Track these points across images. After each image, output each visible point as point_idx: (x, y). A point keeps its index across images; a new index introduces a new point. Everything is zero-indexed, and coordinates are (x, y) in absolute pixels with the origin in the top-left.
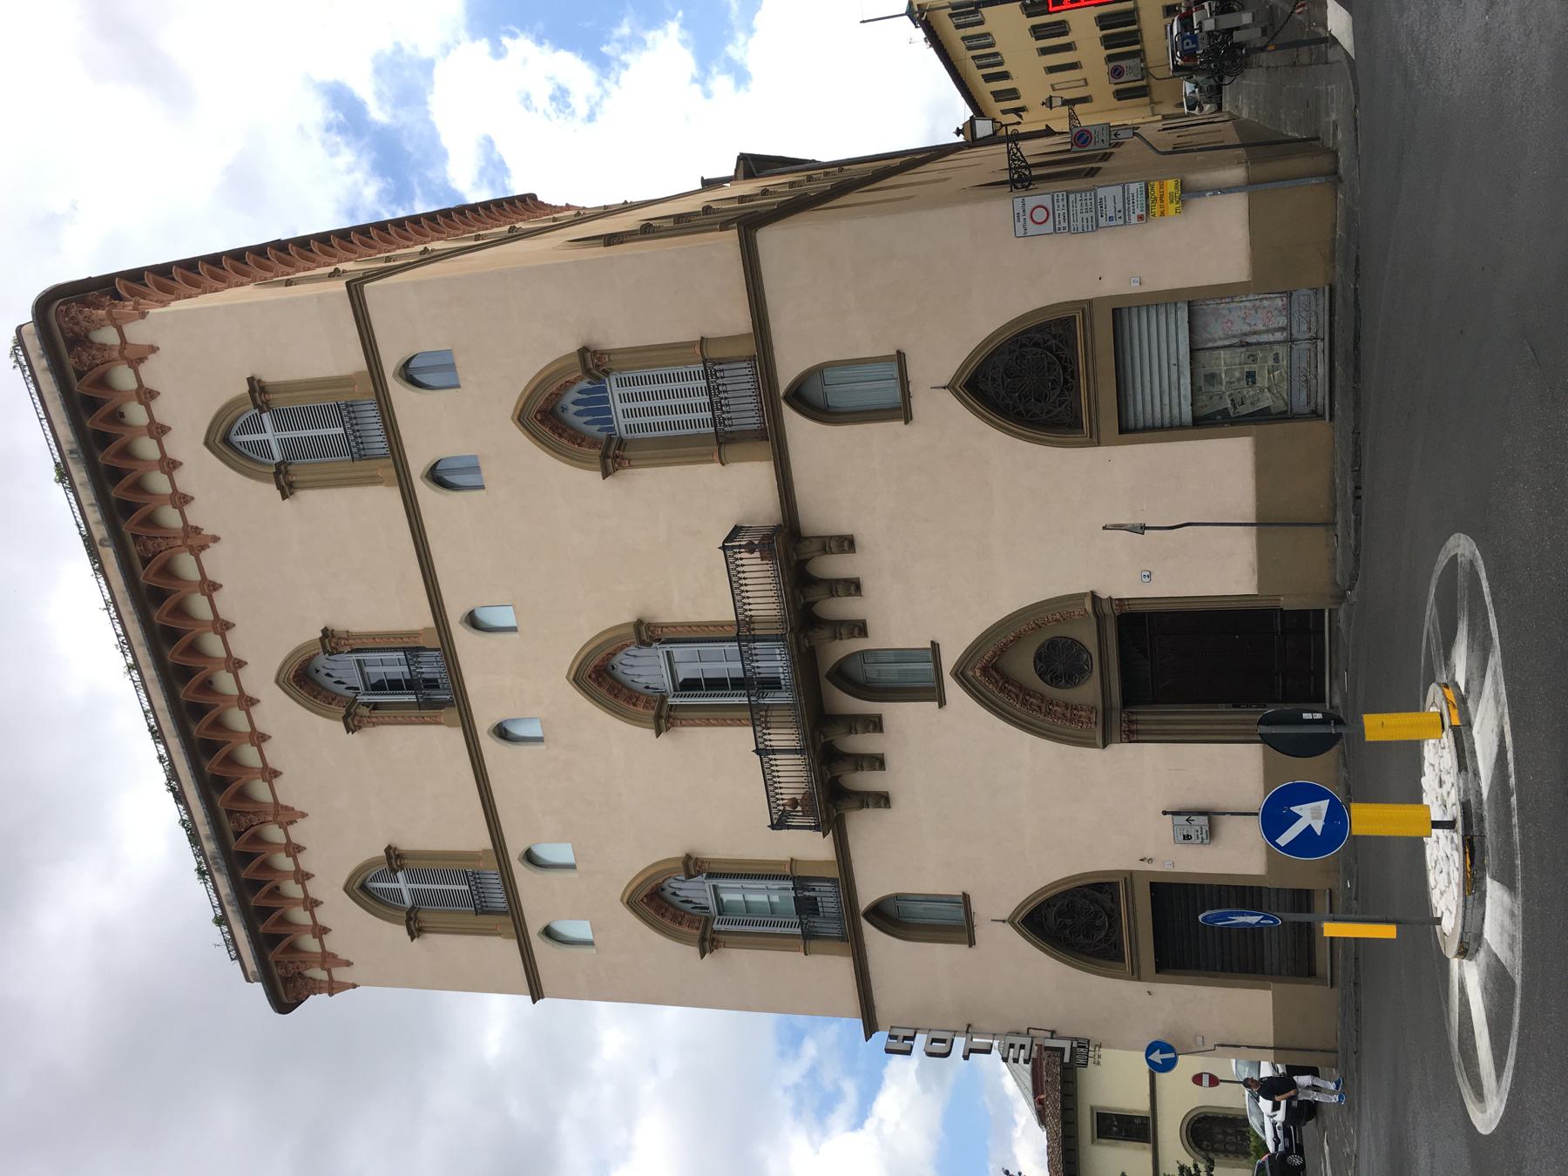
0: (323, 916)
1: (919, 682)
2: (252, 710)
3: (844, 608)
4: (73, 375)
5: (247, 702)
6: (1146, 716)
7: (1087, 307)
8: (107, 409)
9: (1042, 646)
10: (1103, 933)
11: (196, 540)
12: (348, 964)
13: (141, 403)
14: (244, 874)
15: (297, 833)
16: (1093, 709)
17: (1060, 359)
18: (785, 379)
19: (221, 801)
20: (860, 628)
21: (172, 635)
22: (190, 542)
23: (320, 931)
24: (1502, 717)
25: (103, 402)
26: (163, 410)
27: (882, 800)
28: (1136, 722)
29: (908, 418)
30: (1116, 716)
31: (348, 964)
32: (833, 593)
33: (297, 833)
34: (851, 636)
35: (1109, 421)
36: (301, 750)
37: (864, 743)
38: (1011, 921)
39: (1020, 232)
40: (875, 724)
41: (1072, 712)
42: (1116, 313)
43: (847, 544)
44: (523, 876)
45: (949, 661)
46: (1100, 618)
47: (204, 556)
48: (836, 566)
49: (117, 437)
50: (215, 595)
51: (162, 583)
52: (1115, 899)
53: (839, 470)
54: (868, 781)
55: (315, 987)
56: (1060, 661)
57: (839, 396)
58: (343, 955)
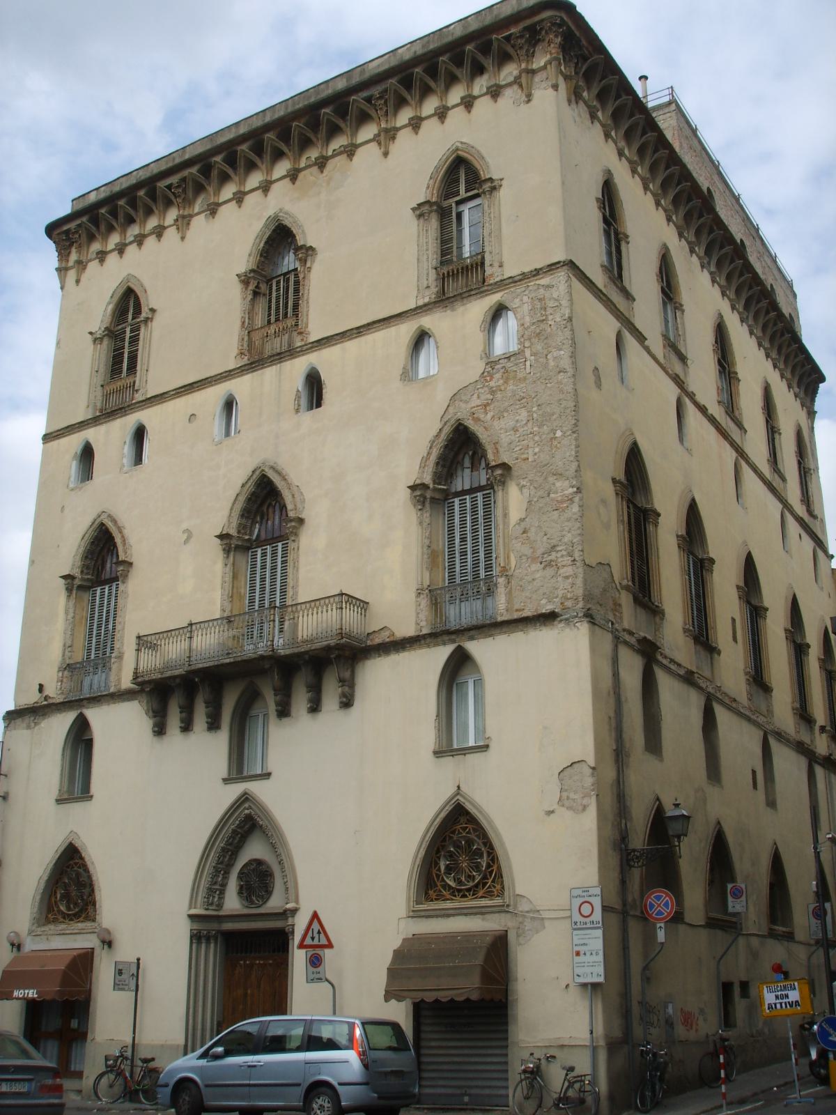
1: (239, 765)
4: (65, 228)
5: (265, 187)
6: (212, 954)
9: (268, 867)
10: (452, 884)
12: (78, 281)
13: (462, 98)
16: (220, 906)
23: (102, 256)
29: (438, 753)
30: (214, 926)
31: (78, 281)
33: (171, 234)
34: (277, 704)
36: (404, 162)
40: (214, 725)
41: (216, 890)
44: (478, 308)
45: (255, 787)
47: (374, 145)
50: (436, 118)
51: (241, 163)
52: (489, 894)
55: (63, 253)
56: (258, 881)
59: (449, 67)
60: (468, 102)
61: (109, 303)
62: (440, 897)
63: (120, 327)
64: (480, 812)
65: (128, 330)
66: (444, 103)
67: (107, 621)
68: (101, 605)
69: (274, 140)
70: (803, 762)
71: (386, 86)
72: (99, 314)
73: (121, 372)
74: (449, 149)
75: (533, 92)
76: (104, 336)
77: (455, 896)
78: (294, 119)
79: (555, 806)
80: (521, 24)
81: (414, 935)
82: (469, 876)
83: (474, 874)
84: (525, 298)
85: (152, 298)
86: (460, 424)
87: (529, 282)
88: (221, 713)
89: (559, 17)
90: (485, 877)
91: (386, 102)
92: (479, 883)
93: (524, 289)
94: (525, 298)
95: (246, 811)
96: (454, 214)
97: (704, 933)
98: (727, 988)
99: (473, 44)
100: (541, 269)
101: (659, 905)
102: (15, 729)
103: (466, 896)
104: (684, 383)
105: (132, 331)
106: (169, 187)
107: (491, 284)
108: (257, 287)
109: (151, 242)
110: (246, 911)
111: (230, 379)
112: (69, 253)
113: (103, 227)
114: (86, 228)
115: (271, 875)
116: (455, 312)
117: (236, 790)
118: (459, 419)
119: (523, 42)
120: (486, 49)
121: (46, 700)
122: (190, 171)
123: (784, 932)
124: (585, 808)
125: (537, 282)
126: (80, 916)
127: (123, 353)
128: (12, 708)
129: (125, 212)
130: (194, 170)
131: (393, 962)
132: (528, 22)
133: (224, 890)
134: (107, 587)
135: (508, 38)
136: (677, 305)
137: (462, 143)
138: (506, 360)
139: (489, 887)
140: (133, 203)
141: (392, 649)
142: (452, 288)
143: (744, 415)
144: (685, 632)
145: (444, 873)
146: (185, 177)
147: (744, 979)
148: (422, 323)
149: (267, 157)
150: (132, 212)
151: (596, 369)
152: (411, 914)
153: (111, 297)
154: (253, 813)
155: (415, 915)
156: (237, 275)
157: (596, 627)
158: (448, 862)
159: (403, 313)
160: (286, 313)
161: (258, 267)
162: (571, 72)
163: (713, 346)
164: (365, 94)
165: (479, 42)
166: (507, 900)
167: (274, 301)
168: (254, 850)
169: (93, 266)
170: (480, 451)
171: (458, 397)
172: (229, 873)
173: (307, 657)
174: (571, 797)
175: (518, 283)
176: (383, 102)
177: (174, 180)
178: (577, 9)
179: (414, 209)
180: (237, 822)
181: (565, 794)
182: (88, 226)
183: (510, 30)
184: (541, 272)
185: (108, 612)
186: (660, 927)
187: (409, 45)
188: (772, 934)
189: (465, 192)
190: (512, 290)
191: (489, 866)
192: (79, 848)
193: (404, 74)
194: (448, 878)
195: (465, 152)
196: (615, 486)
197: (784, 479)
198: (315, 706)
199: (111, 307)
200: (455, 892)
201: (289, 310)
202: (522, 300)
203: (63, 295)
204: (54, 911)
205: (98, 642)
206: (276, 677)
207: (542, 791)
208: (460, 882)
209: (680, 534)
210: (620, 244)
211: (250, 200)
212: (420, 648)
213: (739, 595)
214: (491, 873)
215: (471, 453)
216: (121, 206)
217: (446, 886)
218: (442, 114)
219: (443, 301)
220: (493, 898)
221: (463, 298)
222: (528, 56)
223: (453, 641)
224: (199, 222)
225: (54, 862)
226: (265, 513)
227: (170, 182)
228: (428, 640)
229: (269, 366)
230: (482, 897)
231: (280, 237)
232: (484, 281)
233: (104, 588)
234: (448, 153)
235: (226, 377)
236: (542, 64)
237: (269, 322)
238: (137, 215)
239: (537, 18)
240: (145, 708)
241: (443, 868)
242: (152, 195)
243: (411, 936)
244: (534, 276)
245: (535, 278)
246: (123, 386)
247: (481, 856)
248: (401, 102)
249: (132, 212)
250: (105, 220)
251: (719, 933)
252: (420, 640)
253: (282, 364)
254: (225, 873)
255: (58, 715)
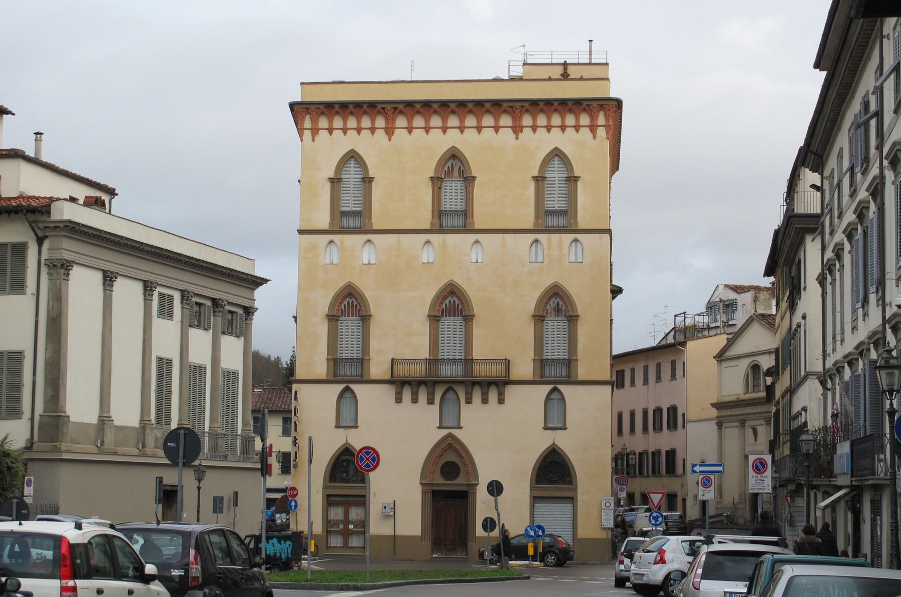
1: (449, 419)
3: (477, 396)
6: (429, 497)
7: (575, 489)
19: (526, 104)
20: (469, 401)
26: (470, 134)
27: (399, 400)
32: (413, 394)
34: (466, 399)
35: (537, 494)
37: (423, 395)
38: (347, 443)
42: (364, 496)
43: (501, 401)
46: (469, 485)
48: (493, 395)
53: (527, 402)
54: (407, 394)
56: (450, 470)
57: (555, 406)
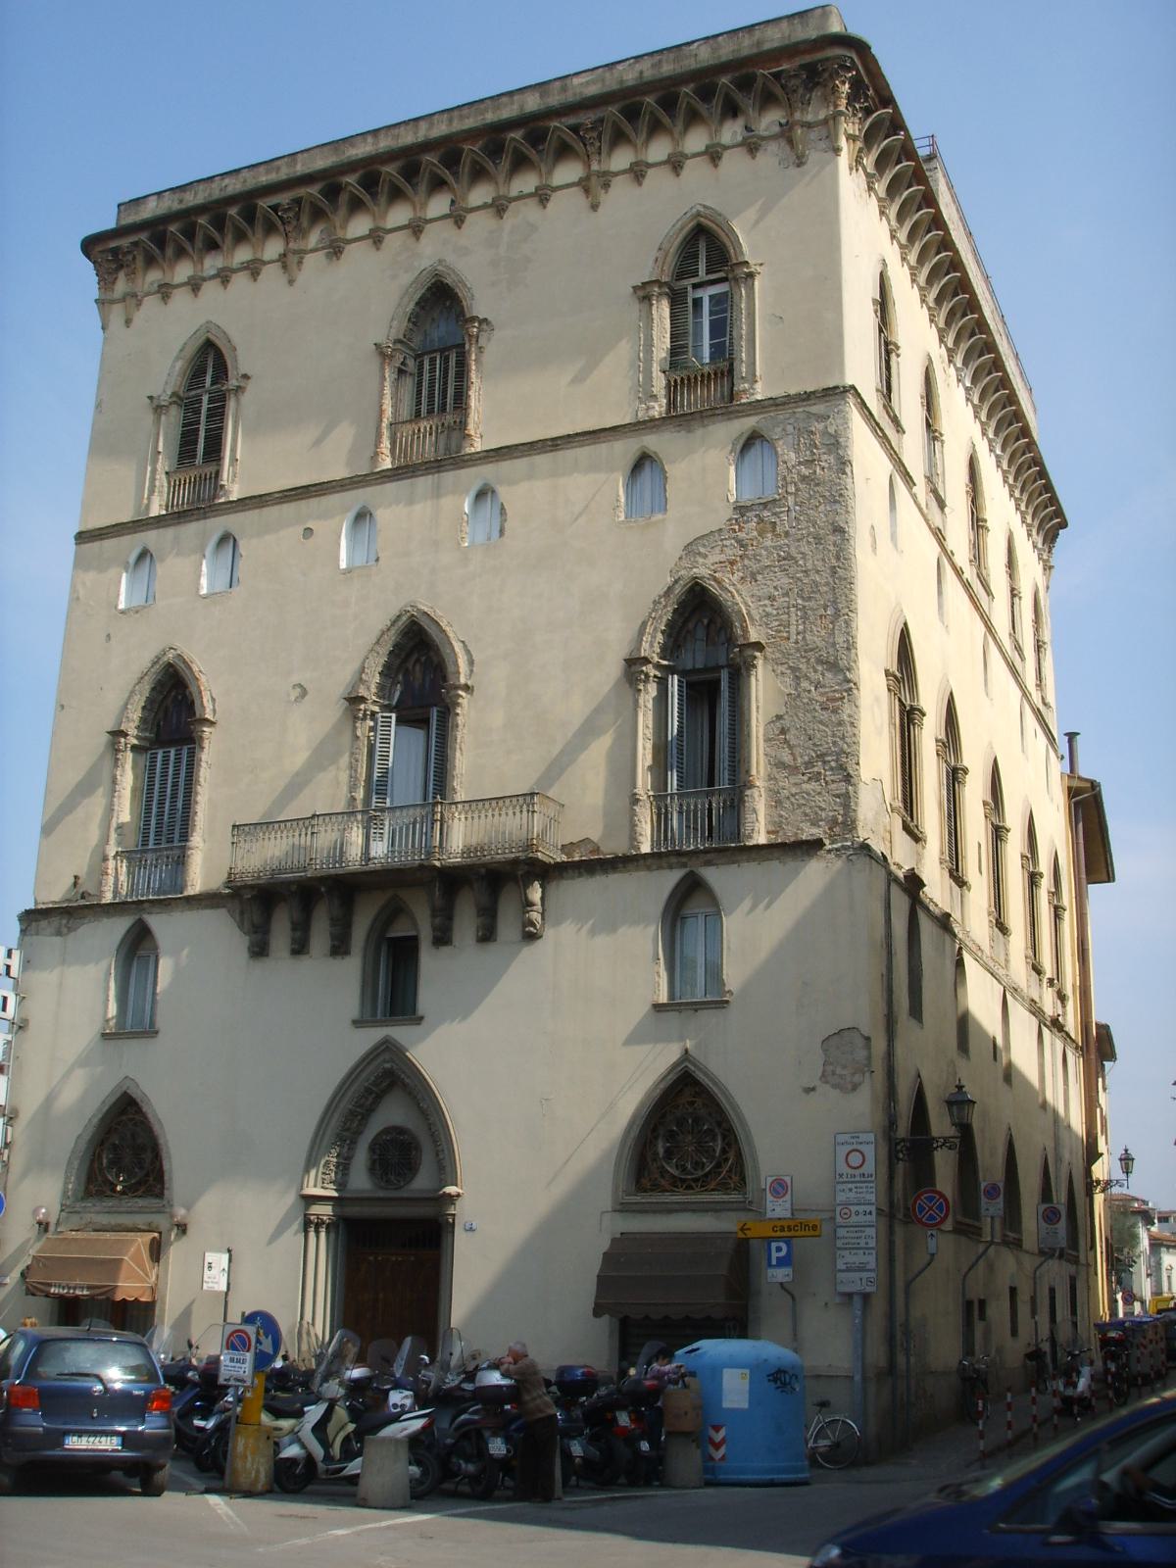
0: (181, 298)
2: (370, 241)
3: (466, 924)
4: (113, 244)
8: (628, 128)
10: (675, 1172)
11: (592, 186)
12: (128, 322)
14: (202, 220)
15: (271, 274)
17: (706, 1175)
18: (713, 875)
20: (442, 938)
21: (411, 172)
22: (594, 179)
23: (165, 291)
24: (1056, 1184)
25: (374, 195)
27: (260, 950)
28: (317, 1232)
31: (128, 322)
33: (271, 274)
34: (434, 929)
36: (639, 208)
39: (841, 1138)
49: (672, 116)
52: (724, 1187)
54: (281, 937)
55: (106, 279)
58: (139, 317)
59: (692, 101)
60: (714, 155)
61: (177, 358)
62: (656, 1188)
63: (193, 393)
64: (715, 1084)
65: (205, 398)
66: (680, 149)
67: (174, 796)
68: (164, 774)
69: (435, 165)
70: (1034, 1021)
71: (602, 115)
72: (165, 372)
73: (194, 456)
74: (685, 214)
75: (807, 152)
76: (171, 404)
77: (677, 1187)
78: (465, 140)
79: (817, 1082)
80: (797, 59)
81: (622, 1234)
82: (697, 1163)
83: (705, 1160)
84: (790, 428)
85: (245, 360)
86: (697, 584)
87: (796, 408)
88: (351, 935)
89: (849, 57)
90: (718, 1165)
91: (600, 134)
92: (710, 1172)
93: (788, 416)
94: (790, 428)
95: (387, 1065)
96: (690, 301)
97: (951, 1237)
98: (969, 1304)
99: (729, 77)
100: (814, 393)
101: (931, 1209)
102: (37, 934)
103: (692, 1188)
104: (945, 540)
105: (210, 401)
106: (275, 208)
107: (744, 404)
108: (403, 363)
109: (240, 281)
110: (381, 1194)
111: (363, 487)
112: (116, 279)
113: (170, 251)
114: (144, 248)
115: (418, 1148)
116: (690, 435)
117: (373, 1036)
118: (696, 578)
119: (797, 83)
120: (745, 84)
121: (83, 897)
122: (309, 190)
123: (1014, 1239)
124: (855, 1087)
125: (806, 409)
126: (137, 1190)
127: (198, 430)
128: (31, 906)
129: (205, 234)
130: (314, 190)
131: (601, 1270)
132: (807, 59)
133: (349, 1164)
134: (173, 752)
135: (777, 76)
136: (937, 434)
137: (704, 206)
138: (761, 507)
139: (724, 1178)
140: (219, 223)
141: (598, 868)
142: (689, 401)
143: (991, 577)
144: (941, 863)
145: (664, 1158)
146: (301, 198)
147: (982, 1297)
148: (645, 444)
149: (423, 188)
150: (216, 235)
151: (873, 527)
152: (619, 1207)
153: (181, 351)
154: (395, 1067)
155: (623, 1208)
156: (375, 344)
157: (873, 861)
158: (668, 1144)
159: (618, 426)
160: (444, 404)
161: (405, 336)
162: (854, 131)
163: (967, 486)
164: (572, 120)
165: (737, 75)
166: (750, 1196)
167: (425, 385)
168: (392, 1114)
169: (151, 303)
170: (719, 621)
171: (694, 547)
172: (355, 1143)
173: (483, 871)
174: (837, 1072)
175: (781, 407)
176: (595, 134)
177: (283, 199)
178: (872, 50)
179: (635, 288)
180: (373, 1078)
181: (830, 1068)
182: (141, 247)
183: (781, 66)
184: (813, 396)
185: (175, 785)
186: (932, 1235)
187: (632, 61)
188: (1005, 1243)
189: (707, 274)
190: (772, 414)
191: (724, 1151)
192: (138, 1100)
193: (628, 102)
194: (668, 1164)
195: (710, 220)
196: (888, 680)
197: (1023, 659)
198: (488, 934)
199: (179, 364)
200: (677, 1184)
201: (448, 400)
202: (784, 430)
203: (105, 339)
204: (97, 1181)
205: (159, 824)
206: (437, 893)
207: (800, 1063)
208: (684, 1170)
209: (940, 737)
210: (889, 357)
211: (393, 242)
212: (637, 870)
213: (985, 813)
214: (727, 1160)
215: (706, 621)
216: (201, 225)
217: (663, 1172)
218: (676, 164)
219: (677, 418)
220: (728, 1191)
221: (702, 417)
222: (803, 104)
223: (684, 865)
224: (314, 262)
225: (100, 1116)
226: (418, 676)
227: (278, 201)
228: (649, 862)
229: (422, 475)
230: (713, 1190)
231: (440, 299)
232: (732, 399)
233: (181, 750)
234: (685, 219)
235: (360, 482)
236: (822, 116)
237: (418, 414)
238: (224, 242)
239: (819, 56)
240: (238, 919)
241: (661, 1151)
242: (250, 215)
243: (619, 1236)
244: (804, 400)
245: (805, 403)
246: (200, 478)
247: (714, 1139)
248: (619, 138)
249: (216, 235)
250: (175, 240)
251: (963, 1239)
252: (637, 861)
253: (442, 474)
254: (351, 1142)
255: (105, 920)
